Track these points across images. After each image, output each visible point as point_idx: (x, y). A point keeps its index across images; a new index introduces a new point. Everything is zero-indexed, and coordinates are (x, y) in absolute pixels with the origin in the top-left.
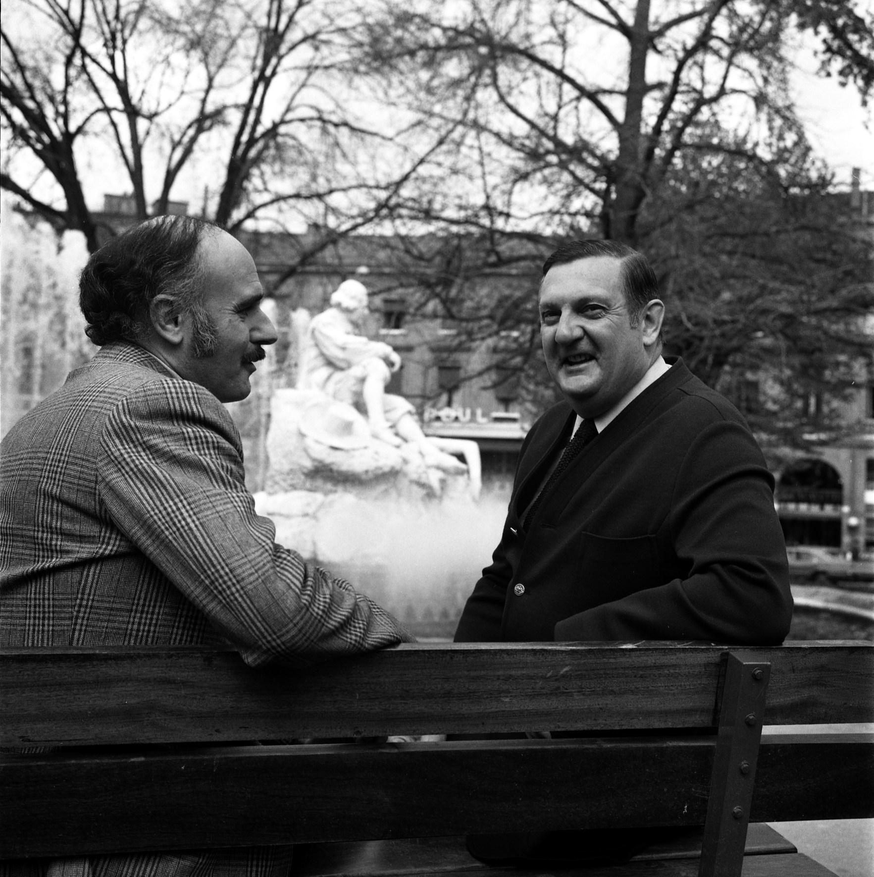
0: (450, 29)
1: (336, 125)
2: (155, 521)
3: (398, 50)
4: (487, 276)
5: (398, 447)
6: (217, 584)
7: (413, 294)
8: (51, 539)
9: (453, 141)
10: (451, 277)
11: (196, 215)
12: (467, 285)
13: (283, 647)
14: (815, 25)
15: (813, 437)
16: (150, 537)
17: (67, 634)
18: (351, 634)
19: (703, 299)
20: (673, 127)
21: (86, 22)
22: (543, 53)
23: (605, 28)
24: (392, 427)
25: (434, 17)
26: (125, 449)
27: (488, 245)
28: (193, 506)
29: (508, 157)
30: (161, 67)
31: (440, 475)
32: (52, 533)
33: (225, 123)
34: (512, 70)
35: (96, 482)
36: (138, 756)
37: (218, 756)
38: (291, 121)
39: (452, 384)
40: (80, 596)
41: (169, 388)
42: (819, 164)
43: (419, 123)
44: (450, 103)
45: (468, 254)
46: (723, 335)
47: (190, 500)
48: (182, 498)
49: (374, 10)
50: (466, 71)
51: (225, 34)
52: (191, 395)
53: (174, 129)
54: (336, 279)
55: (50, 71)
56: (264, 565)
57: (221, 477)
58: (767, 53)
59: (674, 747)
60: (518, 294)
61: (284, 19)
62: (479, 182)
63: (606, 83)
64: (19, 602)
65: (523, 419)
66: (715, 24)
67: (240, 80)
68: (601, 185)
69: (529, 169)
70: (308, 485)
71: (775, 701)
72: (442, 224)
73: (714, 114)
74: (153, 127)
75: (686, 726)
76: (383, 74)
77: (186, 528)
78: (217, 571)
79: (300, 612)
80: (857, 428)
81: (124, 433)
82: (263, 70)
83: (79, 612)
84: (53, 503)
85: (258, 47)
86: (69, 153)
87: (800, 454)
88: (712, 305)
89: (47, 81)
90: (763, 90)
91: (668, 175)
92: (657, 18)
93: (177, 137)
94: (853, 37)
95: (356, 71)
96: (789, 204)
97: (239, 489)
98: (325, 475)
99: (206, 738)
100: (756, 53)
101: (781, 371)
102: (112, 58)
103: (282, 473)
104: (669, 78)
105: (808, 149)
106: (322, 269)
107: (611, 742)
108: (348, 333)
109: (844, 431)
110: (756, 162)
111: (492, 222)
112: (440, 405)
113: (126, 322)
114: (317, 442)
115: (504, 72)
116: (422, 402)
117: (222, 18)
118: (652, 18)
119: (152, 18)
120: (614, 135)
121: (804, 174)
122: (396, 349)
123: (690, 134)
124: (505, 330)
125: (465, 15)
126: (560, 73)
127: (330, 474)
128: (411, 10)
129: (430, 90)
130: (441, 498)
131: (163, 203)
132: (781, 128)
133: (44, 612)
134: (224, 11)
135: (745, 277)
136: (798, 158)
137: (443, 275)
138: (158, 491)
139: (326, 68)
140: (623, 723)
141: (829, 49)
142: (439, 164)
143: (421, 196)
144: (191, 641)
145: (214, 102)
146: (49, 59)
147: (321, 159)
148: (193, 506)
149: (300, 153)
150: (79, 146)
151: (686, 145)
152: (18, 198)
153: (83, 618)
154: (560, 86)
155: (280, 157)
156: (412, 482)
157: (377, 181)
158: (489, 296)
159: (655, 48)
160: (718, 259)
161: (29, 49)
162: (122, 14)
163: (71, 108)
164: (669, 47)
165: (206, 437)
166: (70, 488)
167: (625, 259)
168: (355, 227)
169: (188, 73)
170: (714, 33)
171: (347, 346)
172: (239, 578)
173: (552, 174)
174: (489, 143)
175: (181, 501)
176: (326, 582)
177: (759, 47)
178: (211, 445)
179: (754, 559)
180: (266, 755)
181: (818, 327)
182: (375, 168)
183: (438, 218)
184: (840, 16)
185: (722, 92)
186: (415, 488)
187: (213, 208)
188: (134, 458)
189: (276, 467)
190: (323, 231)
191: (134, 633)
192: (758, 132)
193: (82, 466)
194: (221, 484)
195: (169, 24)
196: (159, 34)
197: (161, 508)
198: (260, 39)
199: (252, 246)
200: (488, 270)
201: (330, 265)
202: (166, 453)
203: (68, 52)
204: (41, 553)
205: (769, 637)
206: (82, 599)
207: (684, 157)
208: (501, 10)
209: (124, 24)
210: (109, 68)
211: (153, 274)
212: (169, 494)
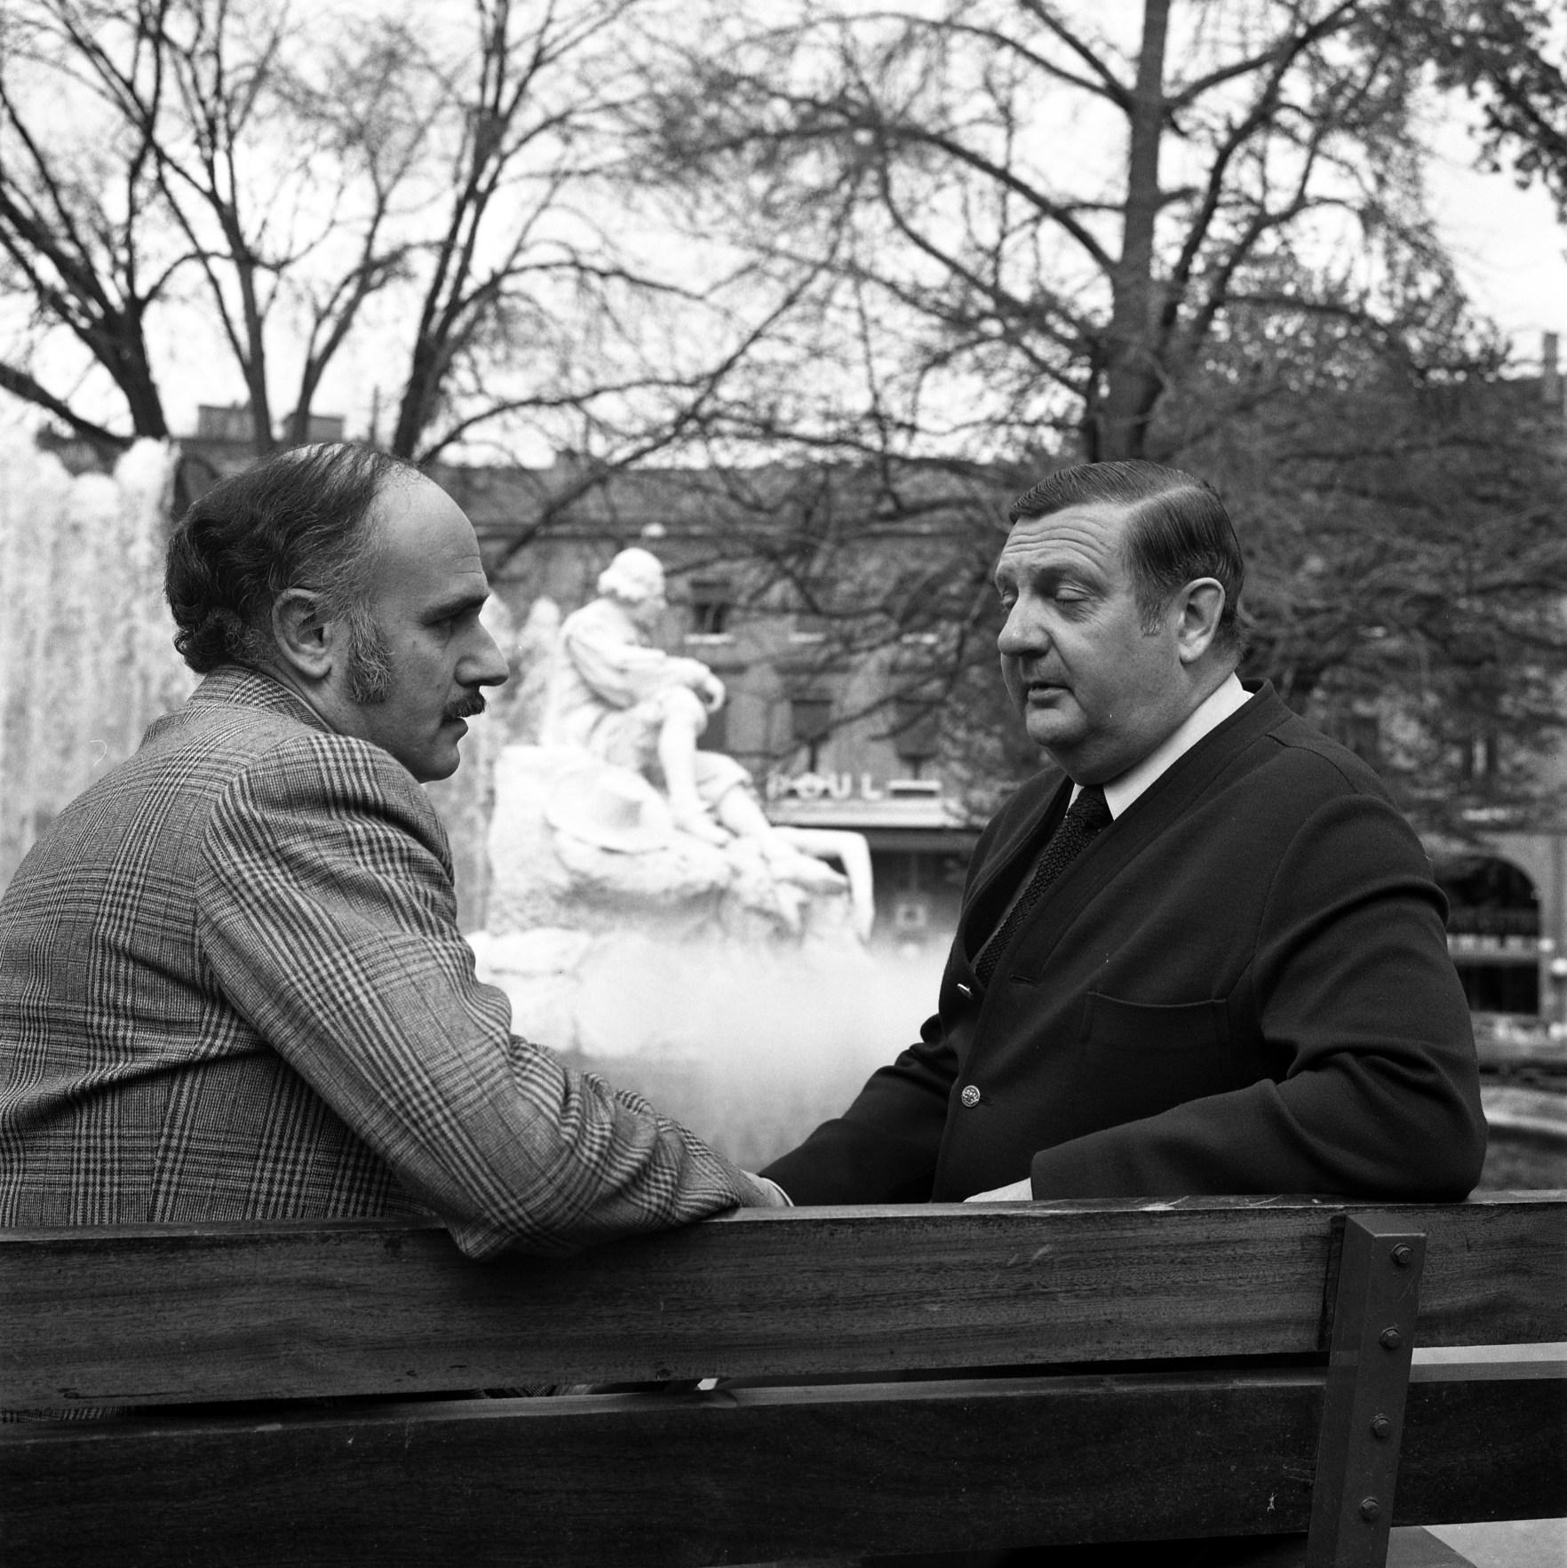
1: (603, 275)
2: (299, 994)
3: (712, 140)
4: (877, 537)
5: (722, 846)
6: (409, 1107)
7: (745, 572)
8: (116, 1028)
9: (813, 299)
10: (812, 540)
11: (359, 440)
12: (841, 554)
13: (529, 1221)
14: (1470, 79)
15: (1483, 815)
17: (143, 1200)
18: (649, 1194)
19: (1275, 571)
20: (1211, 266)
21: (164, 101)
22: (973, 140)
23: (1083, 93)
24: (711, 810)
25: (775, 81)
26: (245, 862)
27: (877, 481)
28: (365, 964)
29: (910, 325)
30: (296, 178)
31: (800, 895)
32: (117, 1016)
33: (408, 276)
34: (915, 171)
35: (195, 923)
36: (270, 1422)
37: (413, 1420)
38: (523, 269)
39: (820, 730)
40: (166, 1130)
41: (323, 751)
42: (1481, 327)
43: (752, 267)
44: (806, 232)
45: (843, 498)
46: (1311, 635)
47: (360, 954)
48: (346, 949)
49: (667, 70)
50: (834, 175)
51: (407, 117)
52: (361, 764)
54: (606, 547)
55: (102, 189)
57: (416, 913)
60: (934, 568)
61: (510, 89)
62: (860, 371)
64: (60, 1143)
65: (946, 791)
66: (1285, 82)
67: (434, 199)
68: (1080, 373)
69: (950, 345)
70: (563, 916)
71: (1434, 1303)
72: (795, 446)
73: (1285, 243)
75: (1270, 1350)
77: (354, 1005)
78: (410, 1083)
79: (558, 1157)
81: (244, 833)
83: (164, 1159)
84: (118, 961)
86: (137, 332)
87: (1457, 847)
89: (97, 208)
90: (1377, 198)
91: (1204, 351)
92: (1178, 73)
93: (324, 302)
94: (1539, 101)
95: (638, 179)
97: (447, 935)
98: (588, 897)
99: (392, 1388)
100: (1361, 131)
101: (1421, 699)
103: (514, 898)
104: (1202, 180)
105: (1460, 301)
106: (581, 530)
107: (1129, 1382)
108: (630, 643)
110: (1365, 325)
111: (885, 441)
112: (795, 768)
113: (234, 627)
114: (578, 840)
115: (903, 176)
116: (764, 764)
117: (400, 90)
118: (1168, 73)
119: (278, 92)
120: (1104, 283)
121: (1454, 345)
122: (716, 670)
123: (1243, 279)
124: (911, 632)
125: (830, 75)
126: (1003, 175)
128: (734, 70)
129: (769, 210)
130: (800, 937)
131: (301, 416)
132: (1410, 264)
134: (403, 76)
136: (1443, 317)
137: (799, 537)
138: (303, 937)
139: (585, 174)
140: (1152, 1346)
141: (1496, 123)
142: (787, 340)
143: (755, 397)
144: (364, 1213)
146: (100, 168)
147: (578, 335)
148: (365, 964)
149: (541, 325)
150: (153, 321)
151: (1236, 299)
152: (48, 416)
153: (172, 1171)
154: (1003, 198)
155: (503, 333)
157: (678, 372)
158: (881, 573)
159: (1174, 127)
161: (66, 153)
162: (228, 85)
163: (139, 253)
164: (1202, 124)
165: (388, 840)
166: (148, 934)
168: (638, 455)
169: (342, 187)
170: (1284, 98)
171: (629, 666)
172: (448, 1096)
173: (993, 354)
174: (877, 301)
175: (344, 956)
176: (602, 1100)
177: (1367, 121)
178: (396, 855)
179: (1417, 1047)
180: (496, 1415)
181: (1487, 618)
182: (673, 350)
183: (787, 436)
184: (1515, 64)
185: (1301, 202)
186: (755, 920)
187: (388, 425)
188: (261, 878)
191: (263, 1198)
192: (1369, 273)
193: (170, 895)
194: (414, 925)
195: (306, 104)
196: (292, 120)
197: (309, 969)
199: (458, 490)
200: (878, 527)
202: (319, 868)
203: (133, 155)
204: (99, 1053)
205: (1448, 1192)
206: (170, 1136)
207: (1232, 320)
208: (895, 65)
209: (230, 103)
210: (205, 184)
211: (286, 544)
212: (322, 943)
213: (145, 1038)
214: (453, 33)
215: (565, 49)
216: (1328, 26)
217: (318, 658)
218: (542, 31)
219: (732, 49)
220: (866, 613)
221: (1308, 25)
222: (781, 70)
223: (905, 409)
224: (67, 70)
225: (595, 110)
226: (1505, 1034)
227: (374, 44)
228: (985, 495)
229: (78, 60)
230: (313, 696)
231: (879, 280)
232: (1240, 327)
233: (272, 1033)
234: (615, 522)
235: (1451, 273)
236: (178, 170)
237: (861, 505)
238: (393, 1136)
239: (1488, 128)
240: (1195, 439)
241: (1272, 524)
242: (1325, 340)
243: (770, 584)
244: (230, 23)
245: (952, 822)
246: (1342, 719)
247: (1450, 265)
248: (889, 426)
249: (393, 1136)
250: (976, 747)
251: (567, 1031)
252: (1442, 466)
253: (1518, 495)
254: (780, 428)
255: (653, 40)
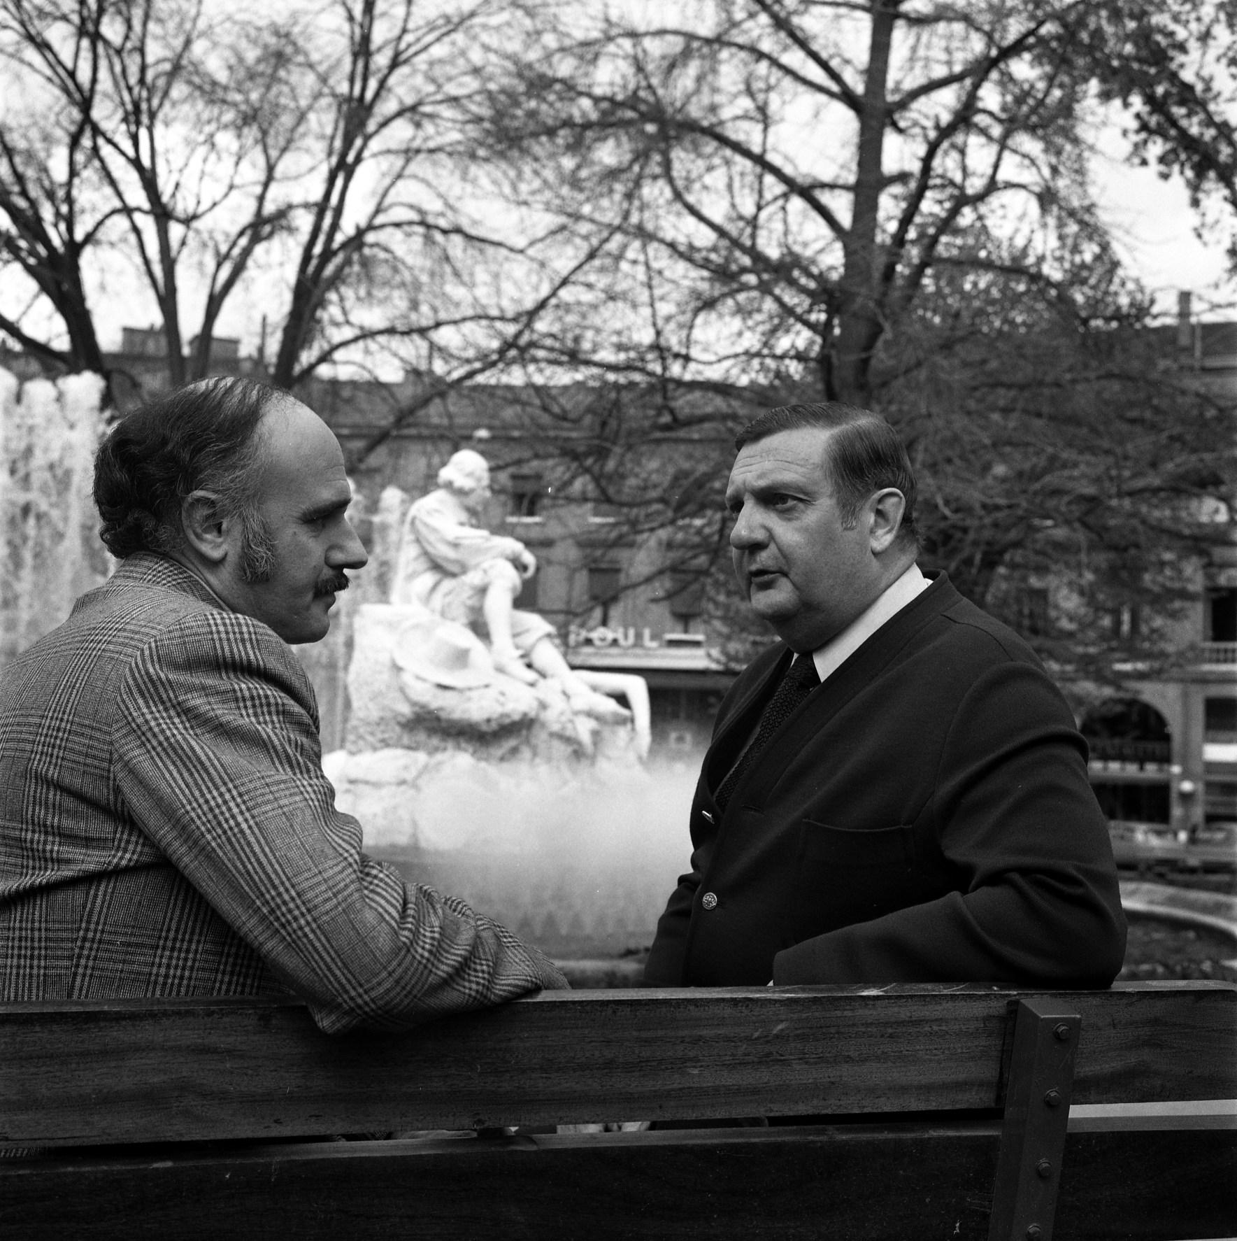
0: (604, 98)
1: (445, 232)
3: (532, 126)
4: (658, 442)
5: (532, 685)
7: (553, 468)
8: (45, 843)
9: (609, 254)
10: (608, 445)
12: (629, 456)
14: (1125, 95)
15: (1127, 667)
16: (186, 841)
17: (64, 981)
19: (968, 475)
20: (922, 235)
21: (99, 87)
22: (739, 132)
23: (822, 98)
24: (523, 656)
25: (582, 83)
27: (658, 399)
29: (685, 277)
30: (202, 150)
32: (46, 833)
33: (291, 230)
34: (692, 156)
35: (110, 761)
37: (278, 1159)
38: (382, 226)
39: (611, 593)
43: (563, 228)
44: (605, 202)
46: (996, 525)
47: (242, 789)
50: (628, 157)
51: (292, 105)
53: (220, 237)
54: (445, 447)
55: (49, 156)
56: (346, 886)
57: (288, 756)
58: (1055, 133)
59: (939, 1138)
60: (703, 468)
61: (373, 84)
62: (646, 311)
63: (826, 173)
65: (709, 642)
66: (982, 92)
67: (312, 169)
69: (716, 293)
70: (406, 740)
71: (1086, 1069)
72: (595, 371)
73: (980, 218)
74: (191, 234)
75: (958, 1107)
76: (511, 162)
78: (279, 894)
80: (1190, 655)
81: (151, 689)
82: (343, 156)
83: (82, 948)
85: (337, 122)
86: (76, 269)
87: (1108, 691)
88: (980, 484)
89: (45, 170)
90: (1051, 184)
91: (916, 301)
92: (898, 83)
93: (224, 249)
94: (1178, 111)
95: (473, 156)
96: (1090, 342)
98: (433, 727)
100: (1040, 132)
101: (1080, 575)
102: (135, 139)
103: (369, 724)
104: (915, 167)
105: (1115, 264)
106: (425, 432)
107: (849, 1131)
108: (462, 524)
109: (1173, 659)
110: (1042, 284)
111: (665, 368)
112: (592, 623)
113: (150, 524)
114: (418, 678)
115: (682, 159)
116: (566, 621)
117: (287, 83)
118: (890, 84)
119: (189, 82)
120: (838, 246)
122: (529, 544)
123: (947, 246)
124: (683, 517)
127: (435, 724)
128: (550, 73)
129: (575, 182)
130: (593, 759)
131: (205, 337)
132: (1077, 236)
133: (33, 948)
134: (289, 72)
135: (1027, 444)
137: (596, 442)
139: (432, 151)
140: (864, 1103)
141: (1144, 127)
142: (589, 286)
143: (564, 331)
144: (242, 992)
145: (274, 201)
146: (47, 138)
147: (424, 278)
149: (395, 270)
154: (760, 178)
156: (553, 735)
157: (502, 310)
160: (987, 418)
162: (150, 75)
163: (77, 207)
164: (915, 124)
165: (267, 697)
167: (836, 430)
170: (980, 105)
172: (310, 905)
174: (661, 258)
175: (229, 791)
178: (273, 709)
179: (1070, 867)
180: (346, 1155)
182: (498, 292)
183: (588, 363)
184: (1159, 83)
185: (992, 186)
186: (557, 745)
187: (273, 346)
189: (361, 714)
190: (427, 380)
191: (161, 980)
193: (91, 738)
195: (213, 92)
196: (200, 105)
197: (201, 801)
198: (339, 110)
200: (658, 435)
201: (437, 427)
203: (73, 129)
205: (1095, 979)
206: (87, 930)
207: (937, 277)
208: (676, 72)
209: (151, 90)
210: (131, 152)
212: (212, 780)
213: (68, 851)
214: (329, 37)
215: (416, 54)
216: (1017, 48)
217: (219, 546)
218: (399, 38)
219: (548, 56)
220: (649, 503)
221: (999, 48)
222: (586, 75)
223: (680, 342)
224: (22, 61)
225: (441, 102)
226: (1144, 839)
227: (266, 46)
228: (742, 412)
229: (31, 54)
230: (212, 579)
231: (662, 241)
232: (943, 283)
233: (170, 851)
234: (451, 427)
235: (1108, 244)
236: (110, 141)
237: (646, 417)
238: (265, 935)
239: (1138, 132)
240: (908, 371)
241: (966, 438)
242: (1009, 293)
243: (573, 478)
244: (152, 26)
245: (714, 666)
246: (1020, 590)
247: (1108, 238)
248: (666, 354)
249: (265, 935)
250: (733, 608)
251: (407, 828)
252: (1099, 393)
253: (1158, 418)
254: (582, 356)
255: (486, 48)
